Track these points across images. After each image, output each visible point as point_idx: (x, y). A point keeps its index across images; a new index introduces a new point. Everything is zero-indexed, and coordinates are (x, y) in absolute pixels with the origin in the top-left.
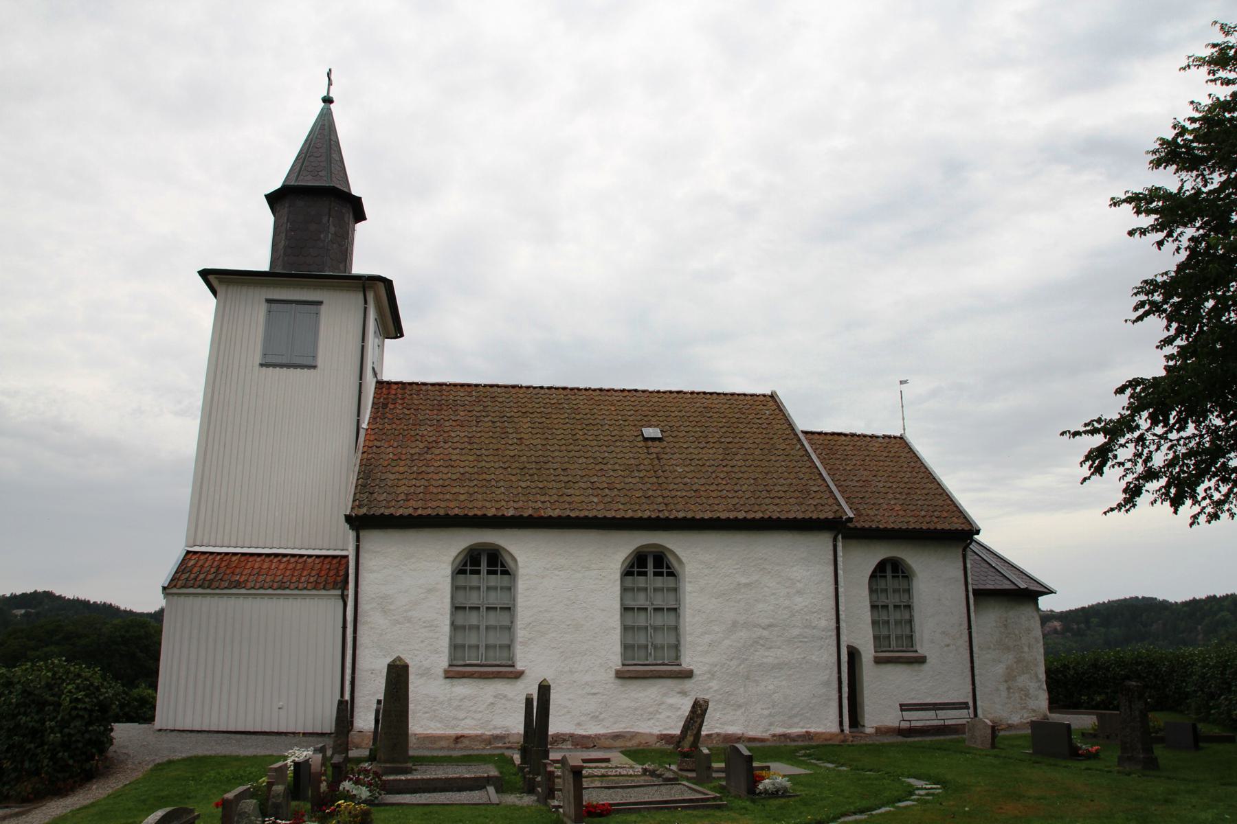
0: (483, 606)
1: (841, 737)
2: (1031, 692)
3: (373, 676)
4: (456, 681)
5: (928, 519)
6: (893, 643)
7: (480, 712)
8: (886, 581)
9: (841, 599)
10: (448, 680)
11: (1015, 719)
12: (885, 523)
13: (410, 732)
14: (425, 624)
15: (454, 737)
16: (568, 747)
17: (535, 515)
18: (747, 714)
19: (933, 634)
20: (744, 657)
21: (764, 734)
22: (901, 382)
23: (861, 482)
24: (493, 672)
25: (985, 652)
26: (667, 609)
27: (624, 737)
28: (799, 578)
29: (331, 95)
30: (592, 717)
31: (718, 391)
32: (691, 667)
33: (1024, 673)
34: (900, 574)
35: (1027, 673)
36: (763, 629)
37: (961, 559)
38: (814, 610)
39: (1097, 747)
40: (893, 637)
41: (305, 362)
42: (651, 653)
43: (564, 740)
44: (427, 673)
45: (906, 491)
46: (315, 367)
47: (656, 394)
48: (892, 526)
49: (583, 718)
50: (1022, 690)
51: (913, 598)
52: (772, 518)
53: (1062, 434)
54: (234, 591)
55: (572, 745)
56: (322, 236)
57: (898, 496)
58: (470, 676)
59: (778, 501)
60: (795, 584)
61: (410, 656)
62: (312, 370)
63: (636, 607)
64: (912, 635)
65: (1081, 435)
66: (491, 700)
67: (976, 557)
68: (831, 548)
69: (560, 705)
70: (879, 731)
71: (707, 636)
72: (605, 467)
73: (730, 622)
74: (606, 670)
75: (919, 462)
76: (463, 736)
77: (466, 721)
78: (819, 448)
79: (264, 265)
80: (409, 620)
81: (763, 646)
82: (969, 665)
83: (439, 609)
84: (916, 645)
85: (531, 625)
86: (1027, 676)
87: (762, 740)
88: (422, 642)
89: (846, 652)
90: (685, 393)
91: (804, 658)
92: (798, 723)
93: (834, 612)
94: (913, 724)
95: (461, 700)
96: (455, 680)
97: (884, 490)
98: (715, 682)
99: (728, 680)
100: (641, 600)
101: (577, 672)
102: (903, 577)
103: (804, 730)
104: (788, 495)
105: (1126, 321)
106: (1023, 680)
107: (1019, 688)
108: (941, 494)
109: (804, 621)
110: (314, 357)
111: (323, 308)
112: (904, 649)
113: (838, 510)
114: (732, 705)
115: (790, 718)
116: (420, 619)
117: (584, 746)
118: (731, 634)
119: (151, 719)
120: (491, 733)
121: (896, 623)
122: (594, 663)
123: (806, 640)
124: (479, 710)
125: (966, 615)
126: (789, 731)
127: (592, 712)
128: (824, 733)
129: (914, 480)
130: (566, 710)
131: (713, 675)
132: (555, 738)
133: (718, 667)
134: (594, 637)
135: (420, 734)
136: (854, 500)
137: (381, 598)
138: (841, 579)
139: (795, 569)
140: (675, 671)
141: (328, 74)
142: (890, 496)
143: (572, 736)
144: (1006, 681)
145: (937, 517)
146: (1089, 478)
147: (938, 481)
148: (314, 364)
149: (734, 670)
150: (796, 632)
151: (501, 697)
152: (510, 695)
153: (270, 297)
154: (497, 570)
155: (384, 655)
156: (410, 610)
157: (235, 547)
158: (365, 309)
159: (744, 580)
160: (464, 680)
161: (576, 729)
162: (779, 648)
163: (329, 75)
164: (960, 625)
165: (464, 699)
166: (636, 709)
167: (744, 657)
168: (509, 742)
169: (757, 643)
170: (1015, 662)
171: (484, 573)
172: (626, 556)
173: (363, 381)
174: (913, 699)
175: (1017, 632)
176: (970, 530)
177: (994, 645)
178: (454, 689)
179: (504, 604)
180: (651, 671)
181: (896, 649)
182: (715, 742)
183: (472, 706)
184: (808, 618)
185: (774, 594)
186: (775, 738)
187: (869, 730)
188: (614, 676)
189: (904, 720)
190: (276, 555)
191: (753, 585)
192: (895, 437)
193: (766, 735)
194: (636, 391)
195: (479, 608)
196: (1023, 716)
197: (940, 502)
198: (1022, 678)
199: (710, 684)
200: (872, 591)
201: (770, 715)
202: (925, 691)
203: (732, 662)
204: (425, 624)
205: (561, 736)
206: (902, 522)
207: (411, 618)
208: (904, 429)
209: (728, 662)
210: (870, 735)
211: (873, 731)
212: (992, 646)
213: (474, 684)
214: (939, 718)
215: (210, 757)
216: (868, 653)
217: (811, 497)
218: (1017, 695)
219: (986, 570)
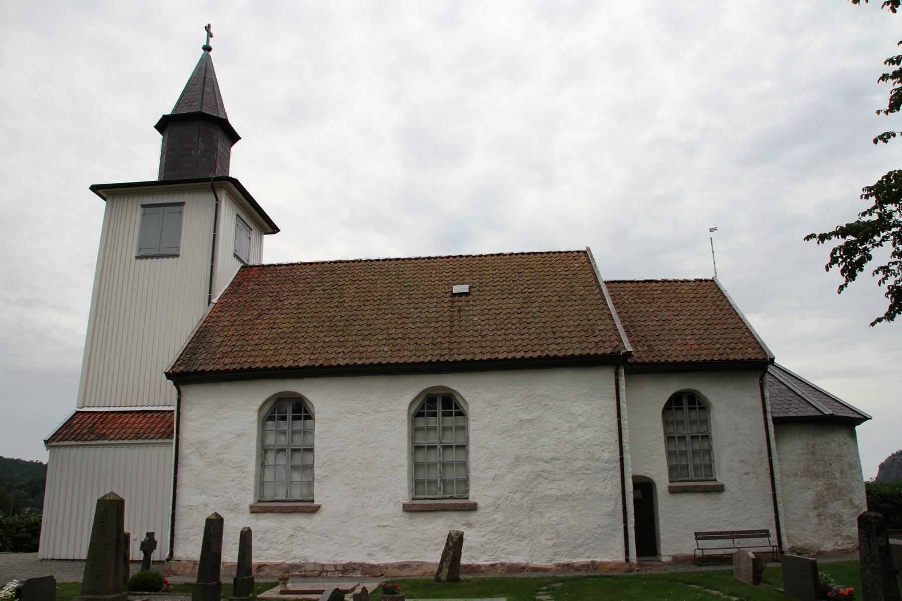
0: (288, 448)
1: (628, 566)
2: (845, 518)
3: (191, 511)
4: (260, 516)
5: (721, 351)
6: (691, 472)
7: (281, 543)
8: (683, 412)
9: (626, 432)
10: (253, 515)
11: (827, 546)
12: (676, 356)
13: (222, 561)
14: (234, 465)
15: (257, 566)
16: (358, 576)
17: (326, 364)
18: (531, 544)
19: (730, 462)
20: (527, 489)
21: (549, 564)
22: (711, 230)
23: (661, 321)
24: (291, 507)
25: (791, 480)
26: (456, 446)
27: (410, 567)
28: (580, 413)
30: (382, 548)
31: (535, 251)
32: (475, 501)
33: (836, 500)
34: (697, 406)
35: (839, 500)
36: (546, 462)
37: (759, 389)
38: (597, 443)
39: (850, 589)
40: (691, 467)
41: (173, 253)
42: (440, 488)
43: (355, 570)
44: (236, 508)
45: (705, 326)
46: (178, 256)
47: (478, 258)
48: (682, 358)
49: (375, 549)
50: (834, 517)
51: (711, 429)
52: (549, 356)
53: (808, 238)
54: (99, 442)
55: (362, 574)
56: (193, 152)
57: (695, 331)
58: (272, 510)
59: (560, 340)
60: (577, 418)
61: (222, 494)
62: (176, 258)
63: (426, 445)
64: (711, 465)
65: (830, 239)
66: (291, 532)
67: (782, 386)
68: (613, 382)
69: (352, 537)
70: (678, 560)
71: (490, 470)
72: (407, 321)
73: (514, 457)
74: (395, 504)
75: (725, 300)
76: (264, 565)
77: (269, 551)
78: (628, 294)
79: (155, 178)
80: (221, 462)
81: (546, 478)
82: (770, 493)
83: (246, 451)
84: (715, 474)
85: (326, 464)
86: (840, 502)
87: (545, 570)
88: (232, 481)
89: (632, 483)
90: (505, 255)
91: (588, 489)
92: (584, 553)
93: (617, 444)
94: (706, 553)
95: (264, 533)
96: (258, 514)
97: (683, 327)
98: (499, 514)
99: (511, 513)
100: (433, 439)
101: (369, 506)
102: (699, 408)
103: (590, 560)
104: (572, 335)
105: (878, 112)
106: (835, 507)
107: (831, 515)
108: (741, 327)
109: (587, 454)
110: (178, 248)
111: (185, 207)
112: (703, 478)
113: (618, 345)
114: (517, 537)
115: (575, 548)
116: (230, 461)
117: (372, 575)
118: (513, 468)
119: (35, 549)
120: (290, 562)
121: (694, 453)
122: (383, 498)
123: (589, 472)
124: (280, 541)
125: (765, 443)
126: (574, 561)
127: (383, 544)
128: (609, 563)
129: (716, 316)
130: (358, 541)
131: (497, 508)
132: (346, 568)
133: (501, 500)
134: (383, 474)
135: (229, 563)
136: (649, 338)
137: (199, 443)
138: (624, 412)
139: (576, 404)
140: (459, 504)
142: (688, 332)
143: (362, 565)
144: (816, 508)
145: (731, 349)
146: (846, 285)
147: (741, 315)
148: (177, 253)
149: (518, 502)
150: (579, 464)
151: (299, 529)
152: (308, 528)
154: (301, 416)
155: (200, 493)
156: (222, 453)
157: (88, 407)
158: (217, 205)
159: (526, 417)
160: (267, 515)
161: (367, 559)
162: (562, 480)
164: (760, 453)
165: (267, 531)
166: (423, 540)
167: (527, 489)
168: (305, 571)
169: (540, 476)
170: (825, 489)
171: (289, 419)
172: (413, 398)
173: (215, 265)
174: (712, 527)
175: (827, 458)
176: (764, 358)
177: (801, 472)
178: (258, 523)
179: (307, 445)
180: (436, 505)
181: (694, 479)
182: (499, 572)
183: (274, 538)
184: (591, 450)
185: (555, 429)
186: (559, 568)
187: (665, 559)
188: (402, 510)
189: (698, 549)
190: (145, 412)
191: (536, 421)
192: (706, 281)
193: (551, 565)
194: (460, 256)
195: (285, 449)
196: (837, 543)
197: (738, 335)
198: (835, 504)
199: (495, 516)
200: (667, 423)
201: (554, 545)
202: (724, 519)
203: (516, 494)
204: (234, 465)
205: (352, 566)
206: (693, 355)
207: (223, 460)
208: (716, 273)
209: (512, 495)
210: (668, 563)
211: (670, 559)
212: (799, 473)
213: (276, 518)
214: (736, 547)
216: (662, 482)
217: (595, 335)
218: (829, 521)
219: (791, 399)
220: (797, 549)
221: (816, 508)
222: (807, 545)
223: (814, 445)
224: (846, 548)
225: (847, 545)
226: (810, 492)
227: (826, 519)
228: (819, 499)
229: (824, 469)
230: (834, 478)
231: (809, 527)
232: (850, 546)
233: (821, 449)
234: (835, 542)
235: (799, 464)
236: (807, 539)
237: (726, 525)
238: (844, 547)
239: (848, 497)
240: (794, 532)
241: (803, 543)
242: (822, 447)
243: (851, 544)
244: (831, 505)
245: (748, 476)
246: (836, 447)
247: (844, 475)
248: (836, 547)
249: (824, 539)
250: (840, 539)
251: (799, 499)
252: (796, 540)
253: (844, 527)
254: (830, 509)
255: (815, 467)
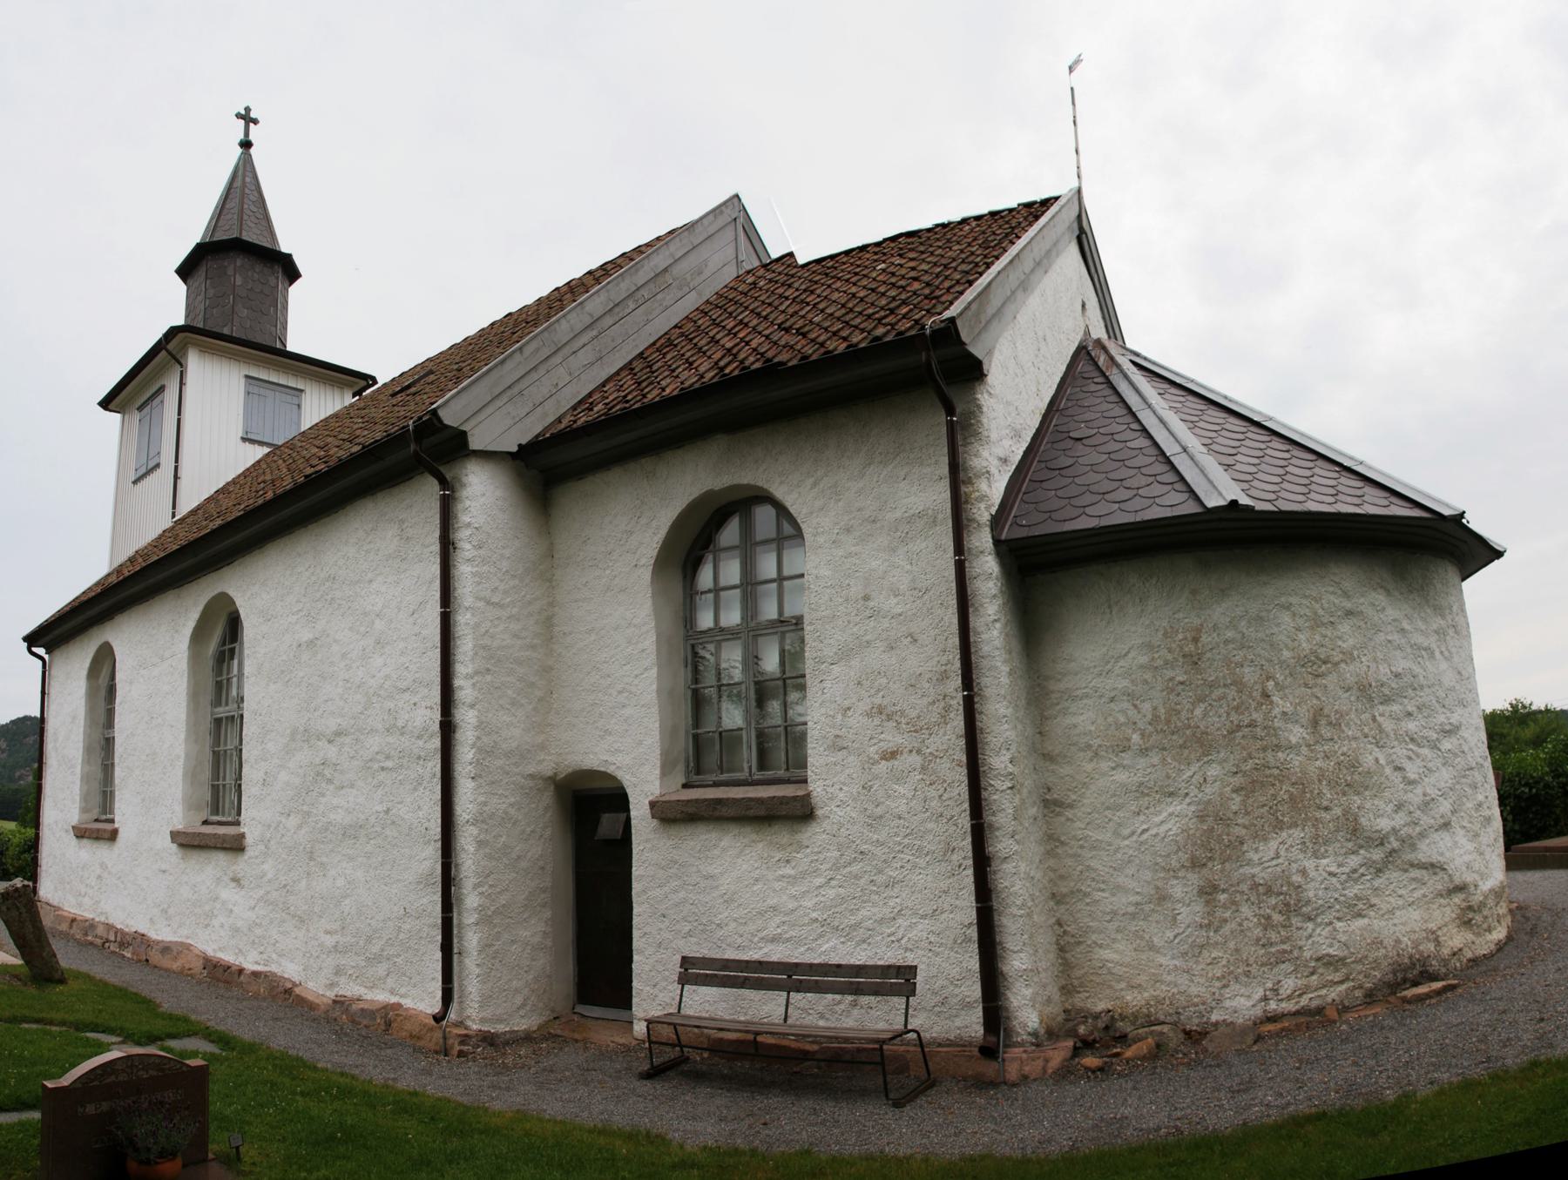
11: (1241, 1003)
19: (840, 717)
25: (1105, 765)
33: (1279, 826)
35: (1294, 825)
37: (944, 441)
50: (1269, 891)
81: (330, 781)
107: (1255, 886)
112: (781, 773)
144: (1195, 864)
170: (1236, 791)
175: (1249, 675)
196: (1275, 991)
198: (1273, 844)
202: (814, 915)
212: (1136, 737)
215: (1487, 729)
220: (1123, 1018)
221: (1195, 864)
222: (1160, 1002)
223: (1199, 630)
224: (1314, 1004)
225: (1324, 992)
226: (1177, 807)
227: (1234, 903)
228: (1212, 830)
229: (1234, 717)
230: (1277, 747)
231: (1170, 934)
232: (1333, 994)
233: (1226, 642)
234: (1269, 985)
235: (1135, 706)
236: (1162, 982)
237: (821, 936)
238: (1304, 1001)
239: (1338, 811)
240: (1115, 957)
241: (1146, 995)
242: (1230, 634)
243: (1342, 982)
244: (1257, 850)
245: (890, 764)
246: (1298, 629)
247: (1326, 732)
248: (1273, 1005)
249: (1226, 980)
250: (1287, 975)
251: (1133, 833)
252: (1123, 985)
253: (1310, 925)
254: (1249, 863)
255: (1198, 712)
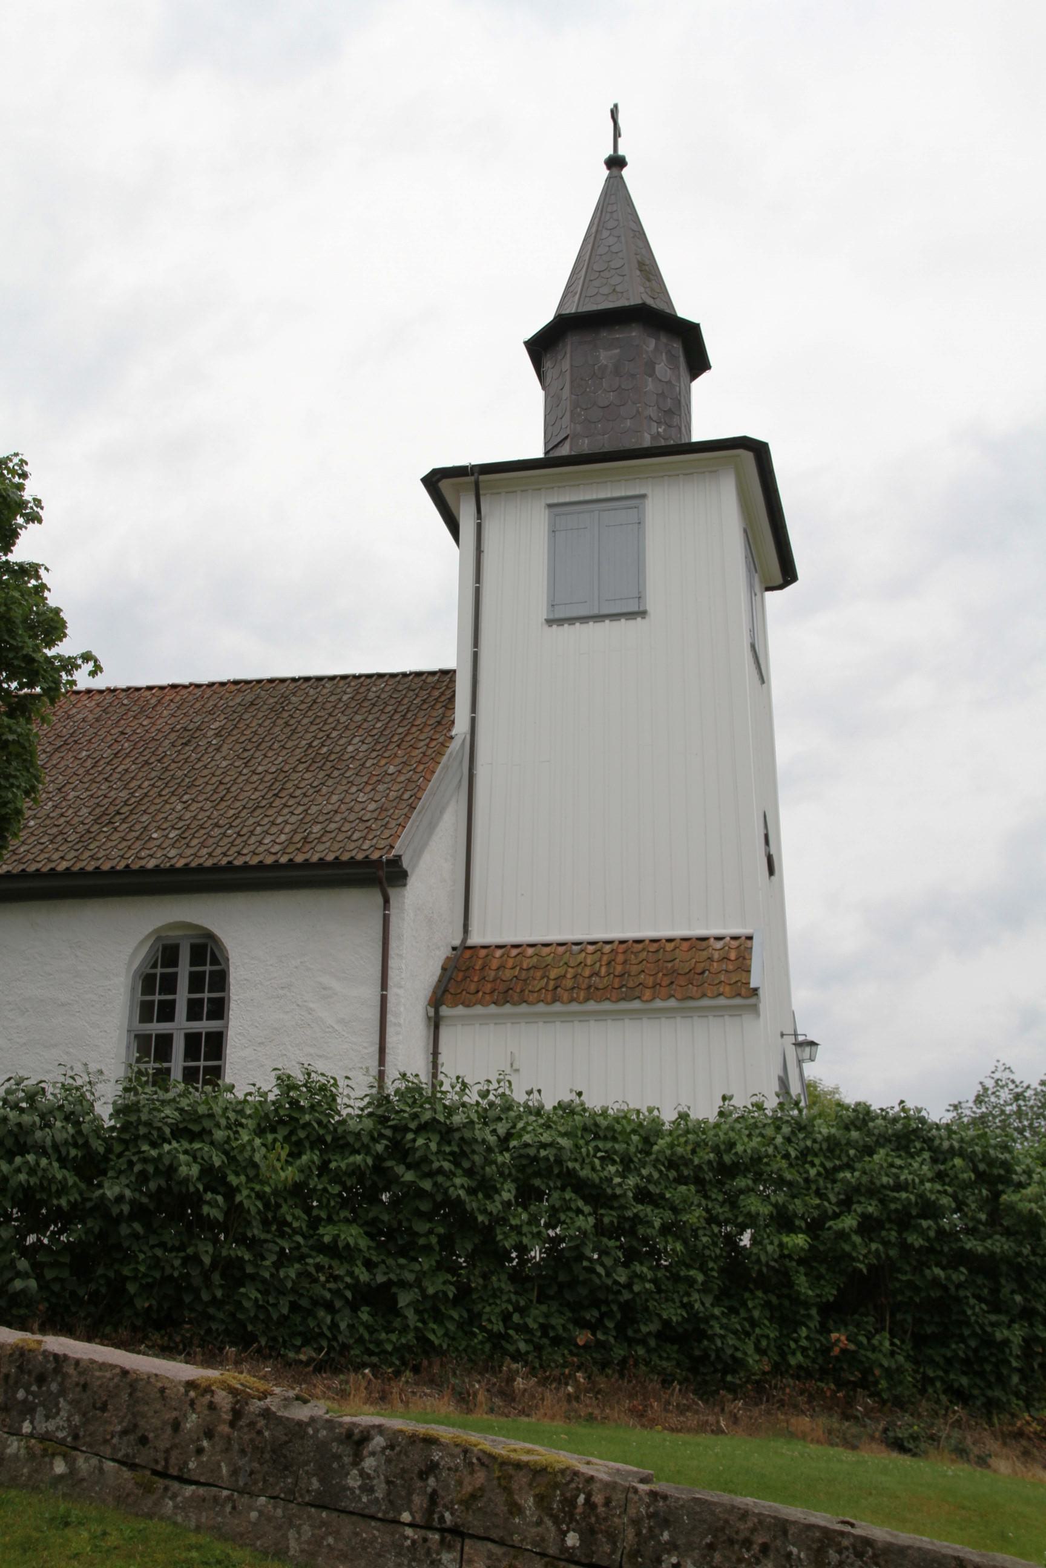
29: (621, 152)
40: (179, 1047)
46: (643, 614)
62: (639, 619)
79: (535, 450)
141: (612, 111)
153: (555, 500)
163: (614, 113)
